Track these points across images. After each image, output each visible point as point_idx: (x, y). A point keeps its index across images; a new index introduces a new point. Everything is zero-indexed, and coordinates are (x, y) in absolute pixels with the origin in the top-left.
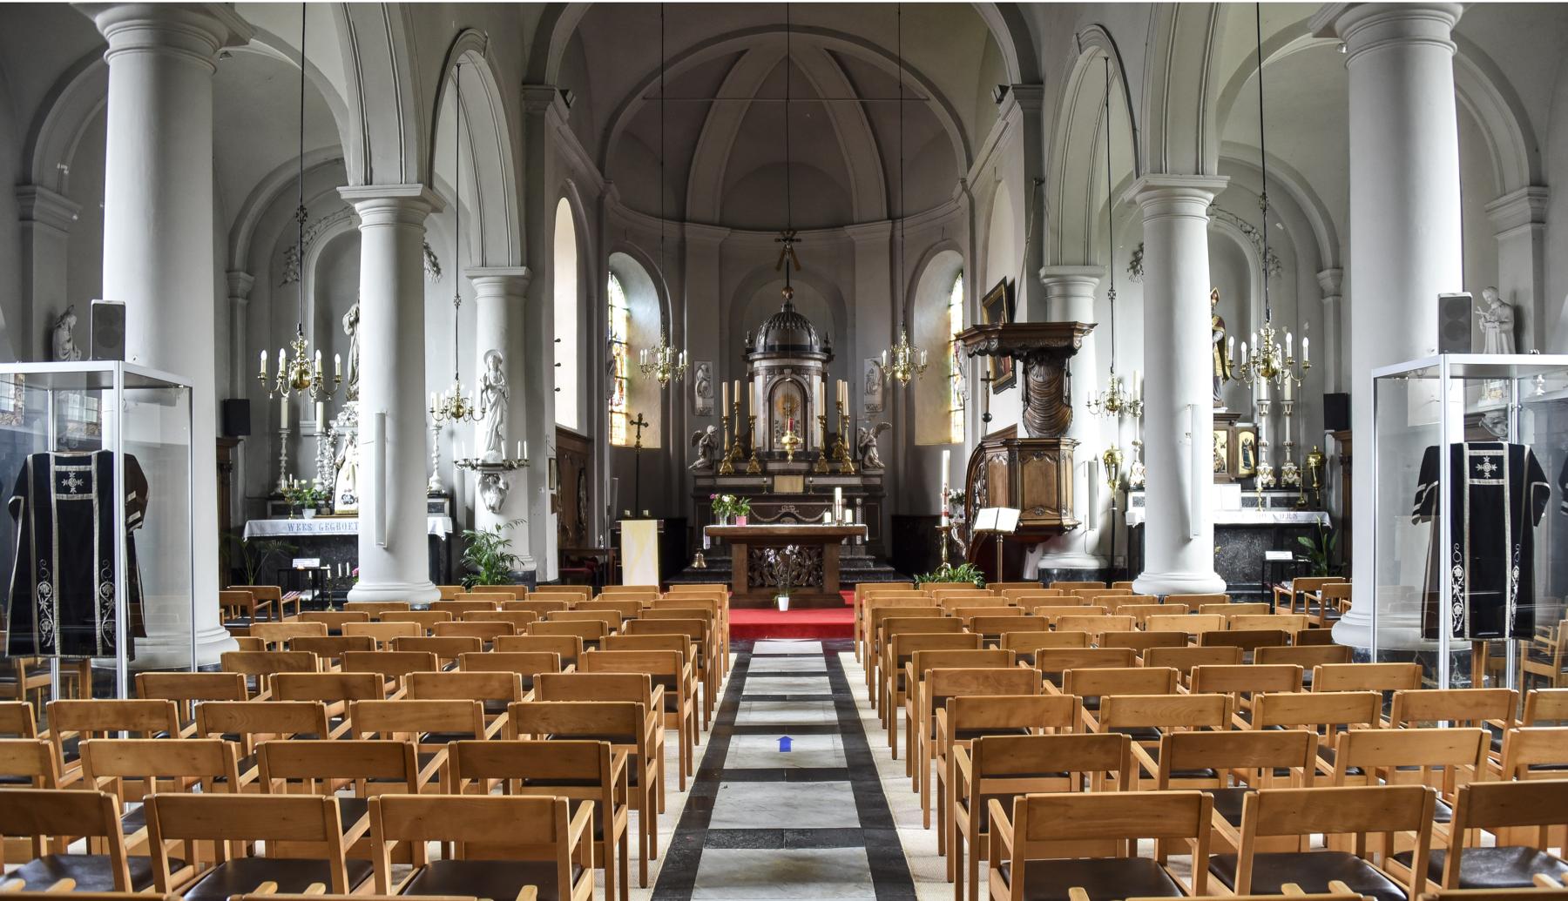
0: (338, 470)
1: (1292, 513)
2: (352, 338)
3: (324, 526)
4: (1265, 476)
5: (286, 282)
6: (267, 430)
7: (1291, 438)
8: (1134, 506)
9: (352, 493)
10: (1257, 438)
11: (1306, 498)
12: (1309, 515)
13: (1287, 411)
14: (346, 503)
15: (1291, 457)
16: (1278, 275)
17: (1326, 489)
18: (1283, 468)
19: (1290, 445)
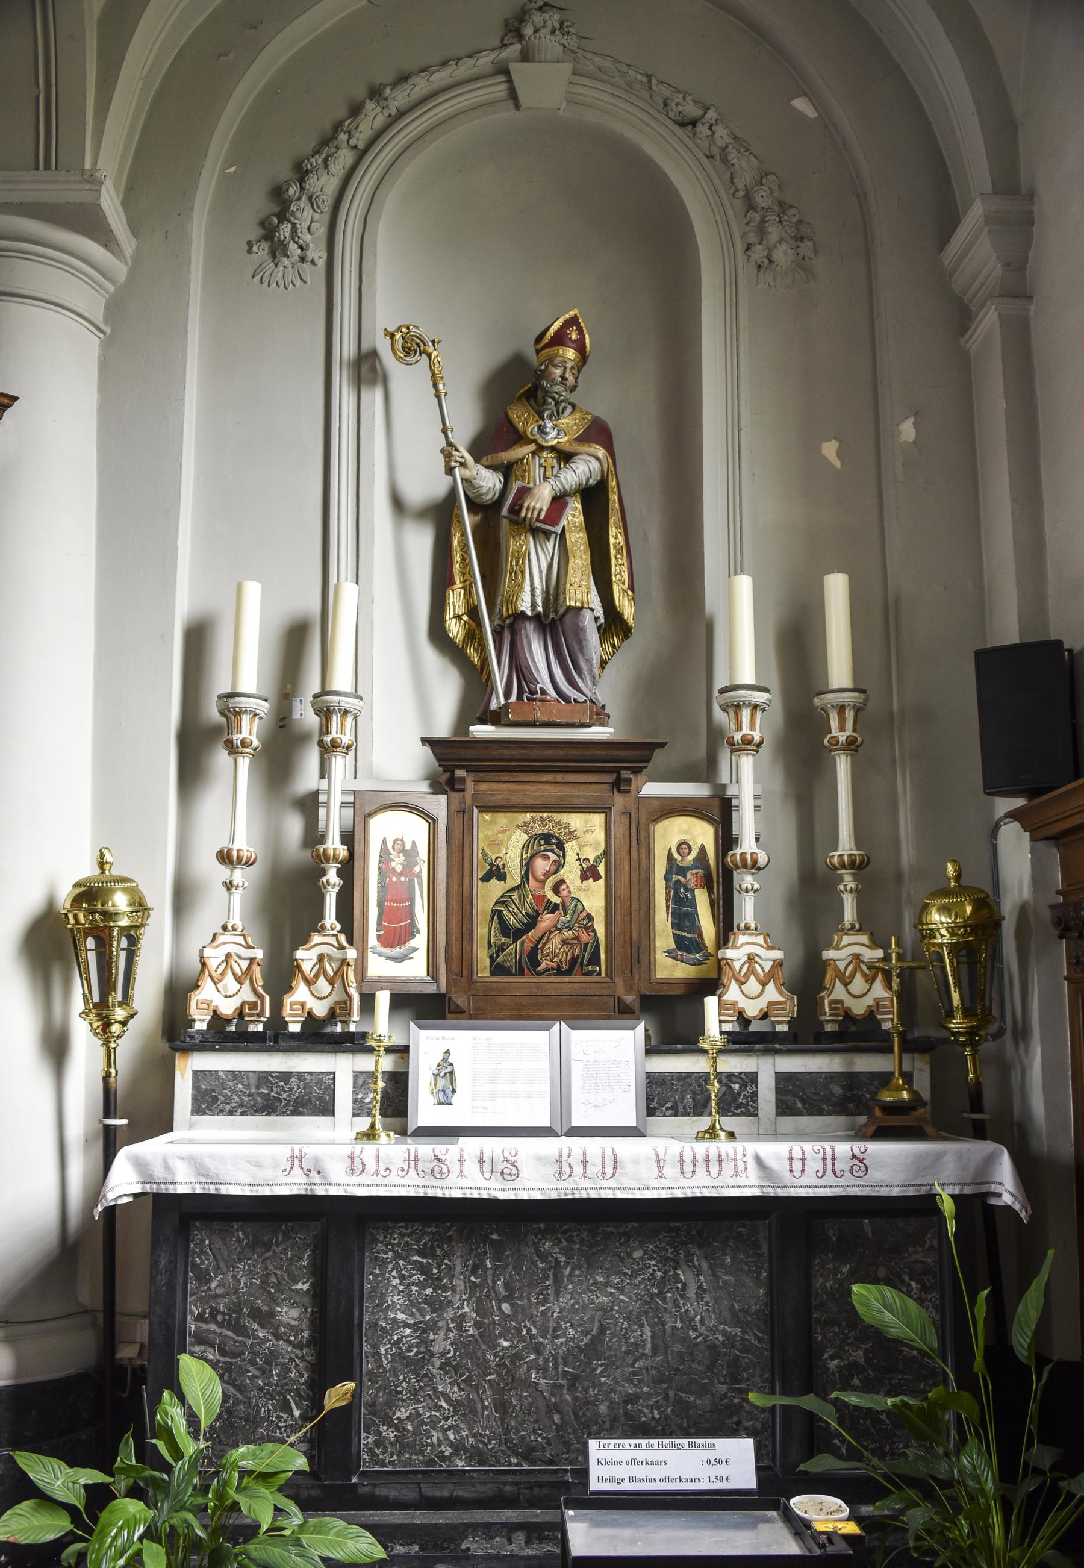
1: (843, 1148)
4: (752, 986)
7: (860, 836)
8: (197, 1110)
10: (727, 840)
11: (923, 1081)
12: (919, 1157)
13: (839, 731)
15: (862, 912)
16: (801, 264)
17: (1008, 1037)
18: (829, 954)
19: (852, 865)
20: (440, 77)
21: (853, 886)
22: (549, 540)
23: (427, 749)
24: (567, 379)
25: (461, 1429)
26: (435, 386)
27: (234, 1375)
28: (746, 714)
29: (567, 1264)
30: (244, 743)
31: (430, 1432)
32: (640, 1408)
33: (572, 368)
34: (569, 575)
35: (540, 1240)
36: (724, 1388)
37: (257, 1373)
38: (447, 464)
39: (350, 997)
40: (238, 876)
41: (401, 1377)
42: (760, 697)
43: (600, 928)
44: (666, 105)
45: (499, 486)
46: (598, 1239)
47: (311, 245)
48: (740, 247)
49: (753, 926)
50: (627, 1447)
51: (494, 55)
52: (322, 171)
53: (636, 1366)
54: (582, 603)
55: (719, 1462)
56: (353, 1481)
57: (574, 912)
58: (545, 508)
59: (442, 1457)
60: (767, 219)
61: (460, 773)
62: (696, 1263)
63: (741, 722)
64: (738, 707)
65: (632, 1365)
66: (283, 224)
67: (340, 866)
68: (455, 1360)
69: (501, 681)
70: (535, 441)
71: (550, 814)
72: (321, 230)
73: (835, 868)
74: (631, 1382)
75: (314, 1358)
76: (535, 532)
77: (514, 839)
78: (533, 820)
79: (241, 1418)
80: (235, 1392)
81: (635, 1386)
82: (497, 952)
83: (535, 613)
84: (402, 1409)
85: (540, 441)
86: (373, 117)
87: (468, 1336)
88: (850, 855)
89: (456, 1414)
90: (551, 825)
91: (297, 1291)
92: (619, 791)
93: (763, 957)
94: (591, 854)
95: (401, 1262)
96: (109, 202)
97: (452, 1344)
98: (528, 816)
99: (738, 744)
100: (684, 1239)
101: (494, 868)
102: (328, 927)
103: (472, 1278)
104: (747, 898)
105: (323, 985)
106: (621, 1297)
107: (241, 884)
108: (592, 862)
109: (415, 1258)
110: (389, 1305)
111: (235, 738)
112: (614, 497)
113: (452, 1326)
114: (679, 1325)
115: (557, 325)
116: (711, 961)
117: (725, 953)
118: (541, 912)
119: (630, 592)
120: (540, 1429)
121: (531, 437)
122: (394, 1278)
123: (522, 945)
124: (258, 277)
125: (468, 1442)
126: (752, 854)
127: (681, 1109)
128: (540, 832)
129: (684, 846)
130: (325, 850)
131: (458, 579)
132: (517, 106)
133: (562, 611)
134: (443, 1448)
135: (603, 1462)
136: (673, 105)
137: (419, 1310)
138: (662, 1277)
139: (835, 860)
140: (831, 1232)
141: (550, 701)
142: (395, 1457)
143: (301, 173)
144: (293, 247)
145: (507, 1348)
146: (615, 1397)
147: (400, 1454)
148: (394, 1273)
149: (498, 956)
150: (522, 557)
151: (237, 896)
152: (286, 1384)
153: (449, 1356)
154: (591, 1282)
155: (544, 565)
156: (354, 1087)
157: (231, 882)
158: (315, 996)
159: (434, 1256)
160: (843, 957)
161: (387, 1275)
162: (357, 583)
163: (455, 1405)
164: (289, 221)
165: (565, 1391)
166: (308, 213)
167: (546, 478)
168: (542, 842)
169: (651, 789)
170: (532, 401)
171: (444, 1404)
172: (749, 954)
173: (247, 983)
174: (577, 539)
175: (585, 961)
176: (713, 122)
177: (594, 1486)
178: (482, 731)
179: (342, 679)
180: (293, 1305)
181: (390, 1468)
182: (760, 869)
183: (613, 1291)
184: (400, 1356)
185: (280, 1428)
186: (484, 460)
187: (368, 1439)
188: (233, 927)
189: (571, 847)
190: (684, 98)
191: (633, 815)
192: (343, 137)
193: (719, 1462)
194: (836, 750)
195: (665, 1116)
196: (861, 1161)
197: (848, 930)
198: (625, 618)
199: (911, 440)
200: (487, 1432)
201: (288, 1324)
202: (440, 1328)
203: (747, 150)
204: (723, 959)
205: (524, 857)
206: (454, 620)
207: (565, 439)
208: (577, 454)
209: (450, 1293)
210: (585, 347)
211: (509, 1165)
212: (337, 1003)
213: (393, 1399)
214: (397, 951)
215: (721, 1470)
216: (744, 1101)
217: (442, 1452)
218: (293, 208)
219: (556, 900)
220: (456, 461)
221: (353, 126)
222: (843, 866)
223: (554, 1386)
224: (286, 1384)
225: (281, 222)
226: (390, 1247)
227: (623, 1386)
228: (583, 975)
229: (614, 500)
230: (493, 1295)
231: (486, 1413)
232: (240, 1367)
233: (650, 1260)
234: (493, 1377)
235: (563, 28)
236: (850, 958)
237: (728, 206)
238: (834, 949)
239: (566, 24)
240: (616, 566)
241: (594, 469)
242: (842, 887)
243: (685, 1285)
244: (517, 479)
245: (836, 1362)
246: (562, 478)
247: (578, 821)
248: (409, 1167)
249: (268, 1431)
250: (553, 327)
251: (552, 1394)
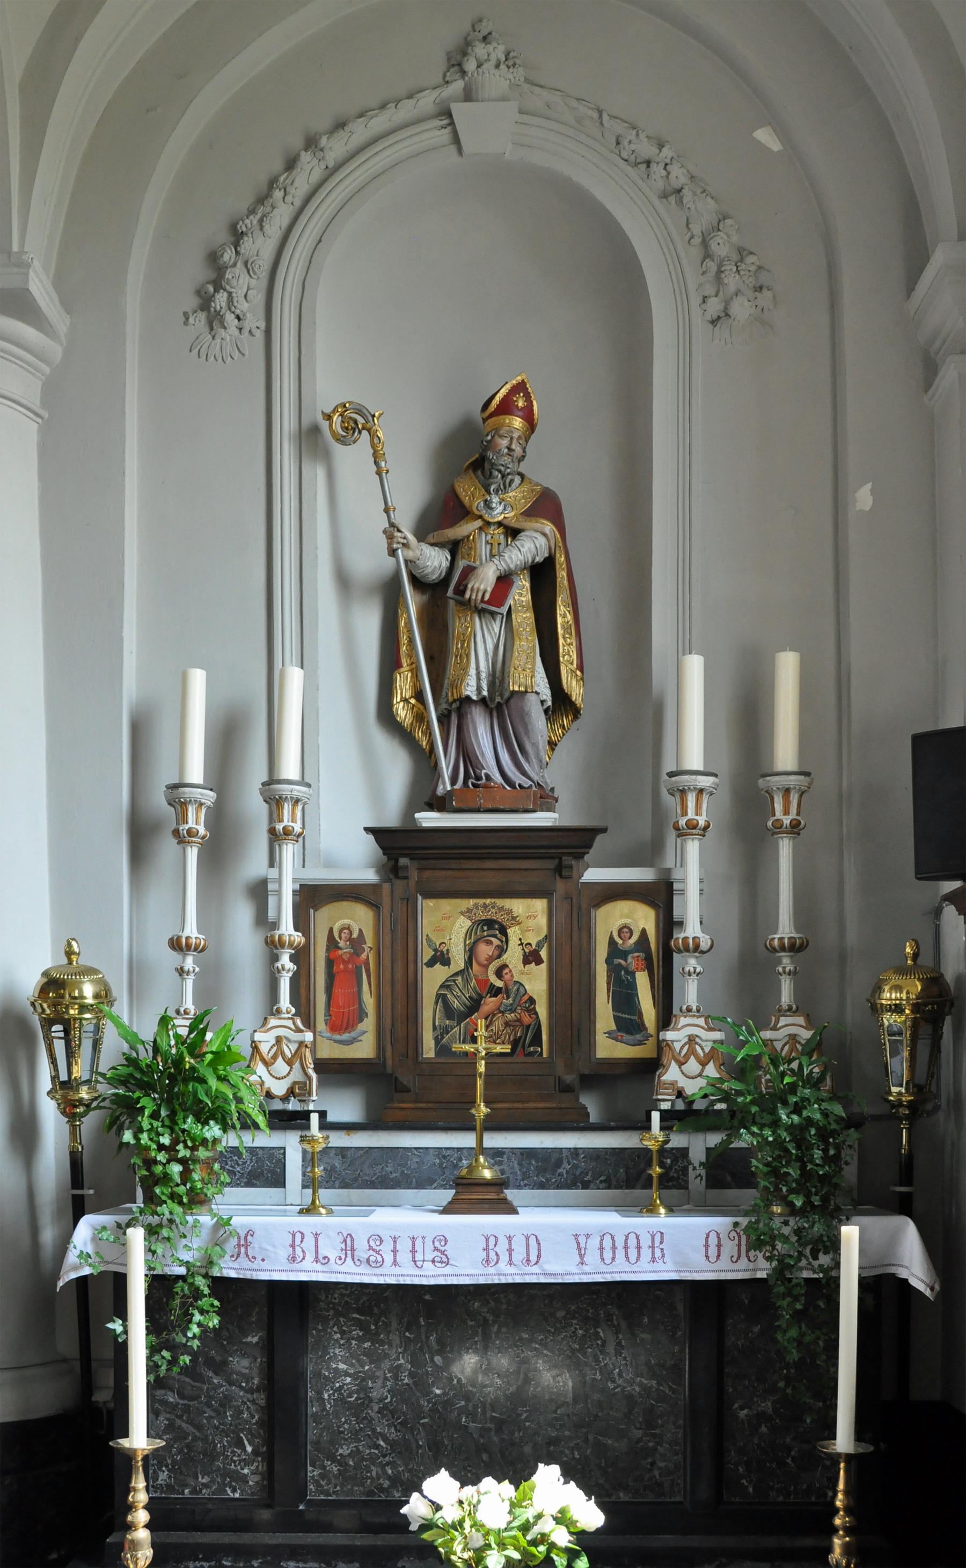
4: (693, 1066)
13: (782, 814)
15: (798, 992)
20: (380, 122)
21: (792, 968)
22: (495, 621)
23: (371, 838)
24: (513, 450)
25: (398, 1464)
26: (376, 463)
27: (192, 1415)
28: (691, 799)
29: (494, 1322)
30: (189, 832)
31: (370, 1467)
32: (562, 1449)
33: (519, 437)
34: (514, 659)
35: (469, 1301)
36: (639, 1433)
37: (213, 1414)
38: (390, 545)
39: (310, 1078)
40: (189, 962)
41: (343, 1420)
42: (705, 782)
43: (542, 1010)
44: (618, 143)
45: (445, 564)
46: (524, 1300)
47: (248, 314)
48: (695, 301)
49: (694, 1008)
51: (435, 94)
52: (257, 233)
53: (558, 1412)
54: (526, 687)
56: (301, 1508)
57: (516, 995)
58: (489, 590)
59: (381, 1489)
60: (723, 269)
61: (403, 861)
62: (615, 1323)
63: (687, 807)
64: (683, 792)
65: (555, 1412)
66: (218, 292)
67: (293, 952)
68: (392, 1405)
69: (447, 768)
70: (480, 517)
71: (493, 900)
72: (258, 297)
73: (774, 950)
74: (553, 1426)
75: (264, 1402)
76: (481, 612)
77: (457, 924)
78: (476, 906)
79: (200, 1453)
80: (194, 1430)
81: (557, 1430)
82: (442, 1035)
83: (480, 697)
84: (344, 1447)
85: (486, 517)
86: (302, 182)
87: (403, 1385)
88: (790, 938)
89: (393, 1451)
90: (494, 911)
91: (247, 1344)
92: (561, 876)
93: (704, 1037)
94: (533, 939)
95: (342, 1319)
96: (39, 284)
97: (389, 1391)
98: (472, 902)
99: (684, 829)
100: (604, 1301)
101: (439, 954)
102: (284, 1010)
103: (407, 1334)
104: (690, 981)
105: (281, 1067)
106: (545, 1352)
107: (191, 969)
108: (534, 947)
109: (354, 1316)
110: (331, 1357)
111: (181, 828)
112: (562, 574)
113: (388, 1375)
114: (598, 1377)
115: (504, 392)
116: (651, 1042)
117: (665, 1035)
118: (484, 995)
119: (579, 673)
120: (469, 1466)
121: (476, 512)
122: (336, 1333)
123: (467, 1025)
124: (195, 351)
125: (404, 1476)
126: (694, 938)
127: (614, 1183)
128: (483, 918)
129: (626, 930)
130: (280, 936)
131: (405, 662)
132: (460, 150)
133: (507, 695)
134: (381, 1481)
136: (625, 143)
137: (358, 1361)
138: (583, 1335)
139: (776, 943)
140: (743, 1296)
141: (493, 787)
142: (338, 1488)
143: (237, 236)
144: (230, 318)
145: (439, 1395)
146: (539, 1439)
147: (342, 1486)
148: (335, 1329)
149: (443, 1038)
150: (468, 638)
151: (189, 983)
152: (239, 1424)
153: (386, 1401)
154: (517, 1338)
155: (490, 647)
156: (303, 1161)
157: (182, 968)
158: (274, 1077)
159: (371, 1313)
160: (780, 1037)
161: (329, 1330)
162: (302, 668)
163: (392, 1444)
164: (225, 290)
165: (493, 1433)
166: (244, 280)
167: (492, 556)
168: (485, 928)
169: (593, 875)
170: (479, 473)
171: (382, 1443)
172: (689, 1036)
173: (297, 1065)
174: (525, 619)
175: (527, 1042)
176: (668, 161)
178: (429, 819)
179: (290, 768)
180: (243, 1356)
181: (334, 1497)
182: (703, 952)
183: (537, 1346)
184: (341, 1402)
185: (235, 1462)
186: (430, 538)
187: (313, 1472)
188: (184, 1011)
189: (514, 933)
190: (637, 135)
191: (574, 901)
192: (278, 194)
194: (779, 833)
195: (598, 1188)
197: (786, 1011)
198: (573, 699)
199: (867, 508)
200: (422, 1468)
201: (240, 1372)
202: (378, 1377)
203: (704, 191)
204: (664, 1040)
205: (467, 942)
206: (402, 704)
207: (512, 514)
208: (523, 530)
209: (386, 1347)
210: (533, 414)
211: (374, 1254)
212: (295, 1083)
213: (336, 1437)
214: (346, 1036)
216: (675, 1175)
217: (382, 1485)
218: (228, 275)
219: (499, 984)
220: (398, 543)
221: (288, 181)
222: (783, 948)
223: (482, 1429)
224: (239, 1424)
225: (216, 290)
226: (331, 1305)
227: (546, 1430)
228: (525, 1055)
229: (563, 576)
230: (427, 1349)
231: (420, 1451)
232: (198, 1409)
233: (573, 1319)
234: (426, 1420)
235: (509, 60)
236: (787, 1038)
237: (682, 255)
238: (771, 1029)
239: (512, 55)
240: (564, 646)
241: (541, 546)
242: (781, 970)
243: (604, 1342)
244: (463, 558)
245: (745, 1411)
246: (507, 558)
247: (521, 907)
249: (224, 1465)
250: (498, 395)
251: (481, 1436)
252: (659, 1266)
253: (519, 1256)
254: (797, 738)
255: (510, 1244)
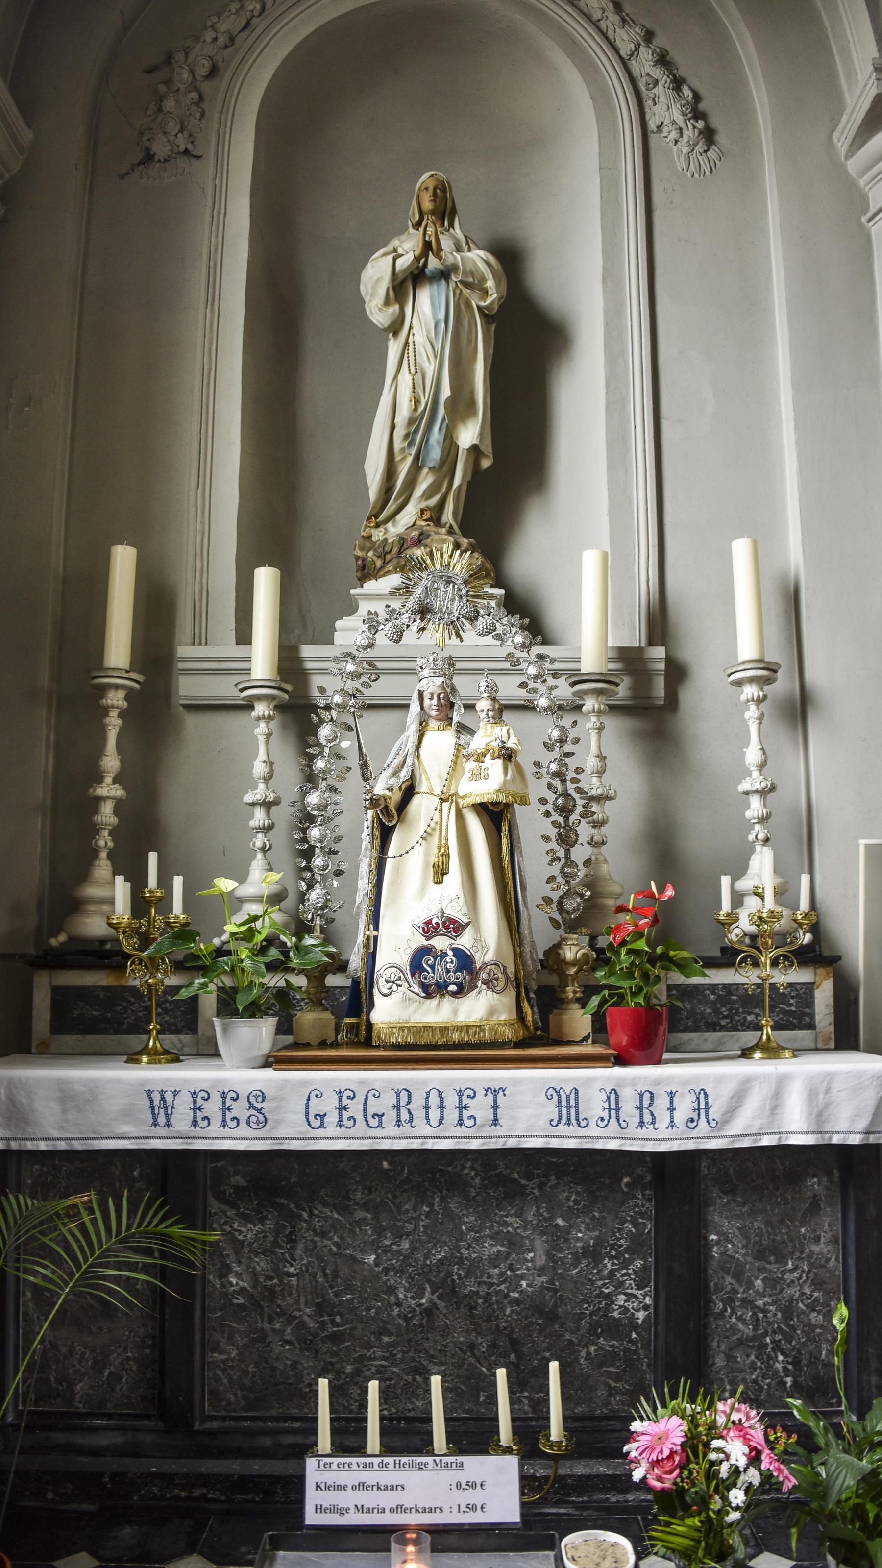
0: (385, 834)
2: (394, 348)
3: (328, 1105)
5: (149, 157)
6: (44, 678)
9: (465, 941)
14: (430, 991)
50: (355, 1467)
55: (472, 1485)
135: (323, 1488)
177: (312, 1518)
193: (472, 1485)
196: (259, 1111)
215: (474, 1497)
248: (699, 1118)
252: (647, 1131)
253: (683, 1111)
254: (108, 613)
255: (672, 1102)
